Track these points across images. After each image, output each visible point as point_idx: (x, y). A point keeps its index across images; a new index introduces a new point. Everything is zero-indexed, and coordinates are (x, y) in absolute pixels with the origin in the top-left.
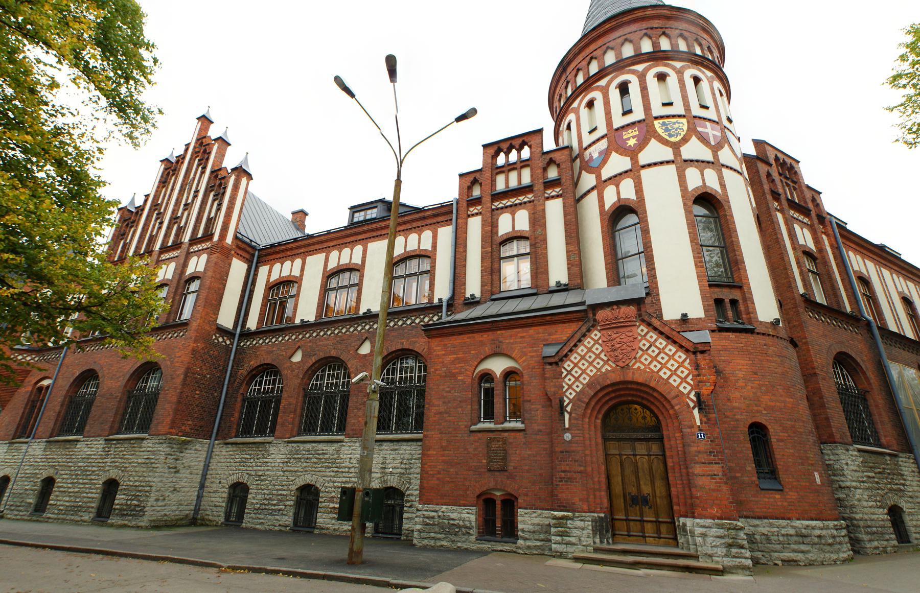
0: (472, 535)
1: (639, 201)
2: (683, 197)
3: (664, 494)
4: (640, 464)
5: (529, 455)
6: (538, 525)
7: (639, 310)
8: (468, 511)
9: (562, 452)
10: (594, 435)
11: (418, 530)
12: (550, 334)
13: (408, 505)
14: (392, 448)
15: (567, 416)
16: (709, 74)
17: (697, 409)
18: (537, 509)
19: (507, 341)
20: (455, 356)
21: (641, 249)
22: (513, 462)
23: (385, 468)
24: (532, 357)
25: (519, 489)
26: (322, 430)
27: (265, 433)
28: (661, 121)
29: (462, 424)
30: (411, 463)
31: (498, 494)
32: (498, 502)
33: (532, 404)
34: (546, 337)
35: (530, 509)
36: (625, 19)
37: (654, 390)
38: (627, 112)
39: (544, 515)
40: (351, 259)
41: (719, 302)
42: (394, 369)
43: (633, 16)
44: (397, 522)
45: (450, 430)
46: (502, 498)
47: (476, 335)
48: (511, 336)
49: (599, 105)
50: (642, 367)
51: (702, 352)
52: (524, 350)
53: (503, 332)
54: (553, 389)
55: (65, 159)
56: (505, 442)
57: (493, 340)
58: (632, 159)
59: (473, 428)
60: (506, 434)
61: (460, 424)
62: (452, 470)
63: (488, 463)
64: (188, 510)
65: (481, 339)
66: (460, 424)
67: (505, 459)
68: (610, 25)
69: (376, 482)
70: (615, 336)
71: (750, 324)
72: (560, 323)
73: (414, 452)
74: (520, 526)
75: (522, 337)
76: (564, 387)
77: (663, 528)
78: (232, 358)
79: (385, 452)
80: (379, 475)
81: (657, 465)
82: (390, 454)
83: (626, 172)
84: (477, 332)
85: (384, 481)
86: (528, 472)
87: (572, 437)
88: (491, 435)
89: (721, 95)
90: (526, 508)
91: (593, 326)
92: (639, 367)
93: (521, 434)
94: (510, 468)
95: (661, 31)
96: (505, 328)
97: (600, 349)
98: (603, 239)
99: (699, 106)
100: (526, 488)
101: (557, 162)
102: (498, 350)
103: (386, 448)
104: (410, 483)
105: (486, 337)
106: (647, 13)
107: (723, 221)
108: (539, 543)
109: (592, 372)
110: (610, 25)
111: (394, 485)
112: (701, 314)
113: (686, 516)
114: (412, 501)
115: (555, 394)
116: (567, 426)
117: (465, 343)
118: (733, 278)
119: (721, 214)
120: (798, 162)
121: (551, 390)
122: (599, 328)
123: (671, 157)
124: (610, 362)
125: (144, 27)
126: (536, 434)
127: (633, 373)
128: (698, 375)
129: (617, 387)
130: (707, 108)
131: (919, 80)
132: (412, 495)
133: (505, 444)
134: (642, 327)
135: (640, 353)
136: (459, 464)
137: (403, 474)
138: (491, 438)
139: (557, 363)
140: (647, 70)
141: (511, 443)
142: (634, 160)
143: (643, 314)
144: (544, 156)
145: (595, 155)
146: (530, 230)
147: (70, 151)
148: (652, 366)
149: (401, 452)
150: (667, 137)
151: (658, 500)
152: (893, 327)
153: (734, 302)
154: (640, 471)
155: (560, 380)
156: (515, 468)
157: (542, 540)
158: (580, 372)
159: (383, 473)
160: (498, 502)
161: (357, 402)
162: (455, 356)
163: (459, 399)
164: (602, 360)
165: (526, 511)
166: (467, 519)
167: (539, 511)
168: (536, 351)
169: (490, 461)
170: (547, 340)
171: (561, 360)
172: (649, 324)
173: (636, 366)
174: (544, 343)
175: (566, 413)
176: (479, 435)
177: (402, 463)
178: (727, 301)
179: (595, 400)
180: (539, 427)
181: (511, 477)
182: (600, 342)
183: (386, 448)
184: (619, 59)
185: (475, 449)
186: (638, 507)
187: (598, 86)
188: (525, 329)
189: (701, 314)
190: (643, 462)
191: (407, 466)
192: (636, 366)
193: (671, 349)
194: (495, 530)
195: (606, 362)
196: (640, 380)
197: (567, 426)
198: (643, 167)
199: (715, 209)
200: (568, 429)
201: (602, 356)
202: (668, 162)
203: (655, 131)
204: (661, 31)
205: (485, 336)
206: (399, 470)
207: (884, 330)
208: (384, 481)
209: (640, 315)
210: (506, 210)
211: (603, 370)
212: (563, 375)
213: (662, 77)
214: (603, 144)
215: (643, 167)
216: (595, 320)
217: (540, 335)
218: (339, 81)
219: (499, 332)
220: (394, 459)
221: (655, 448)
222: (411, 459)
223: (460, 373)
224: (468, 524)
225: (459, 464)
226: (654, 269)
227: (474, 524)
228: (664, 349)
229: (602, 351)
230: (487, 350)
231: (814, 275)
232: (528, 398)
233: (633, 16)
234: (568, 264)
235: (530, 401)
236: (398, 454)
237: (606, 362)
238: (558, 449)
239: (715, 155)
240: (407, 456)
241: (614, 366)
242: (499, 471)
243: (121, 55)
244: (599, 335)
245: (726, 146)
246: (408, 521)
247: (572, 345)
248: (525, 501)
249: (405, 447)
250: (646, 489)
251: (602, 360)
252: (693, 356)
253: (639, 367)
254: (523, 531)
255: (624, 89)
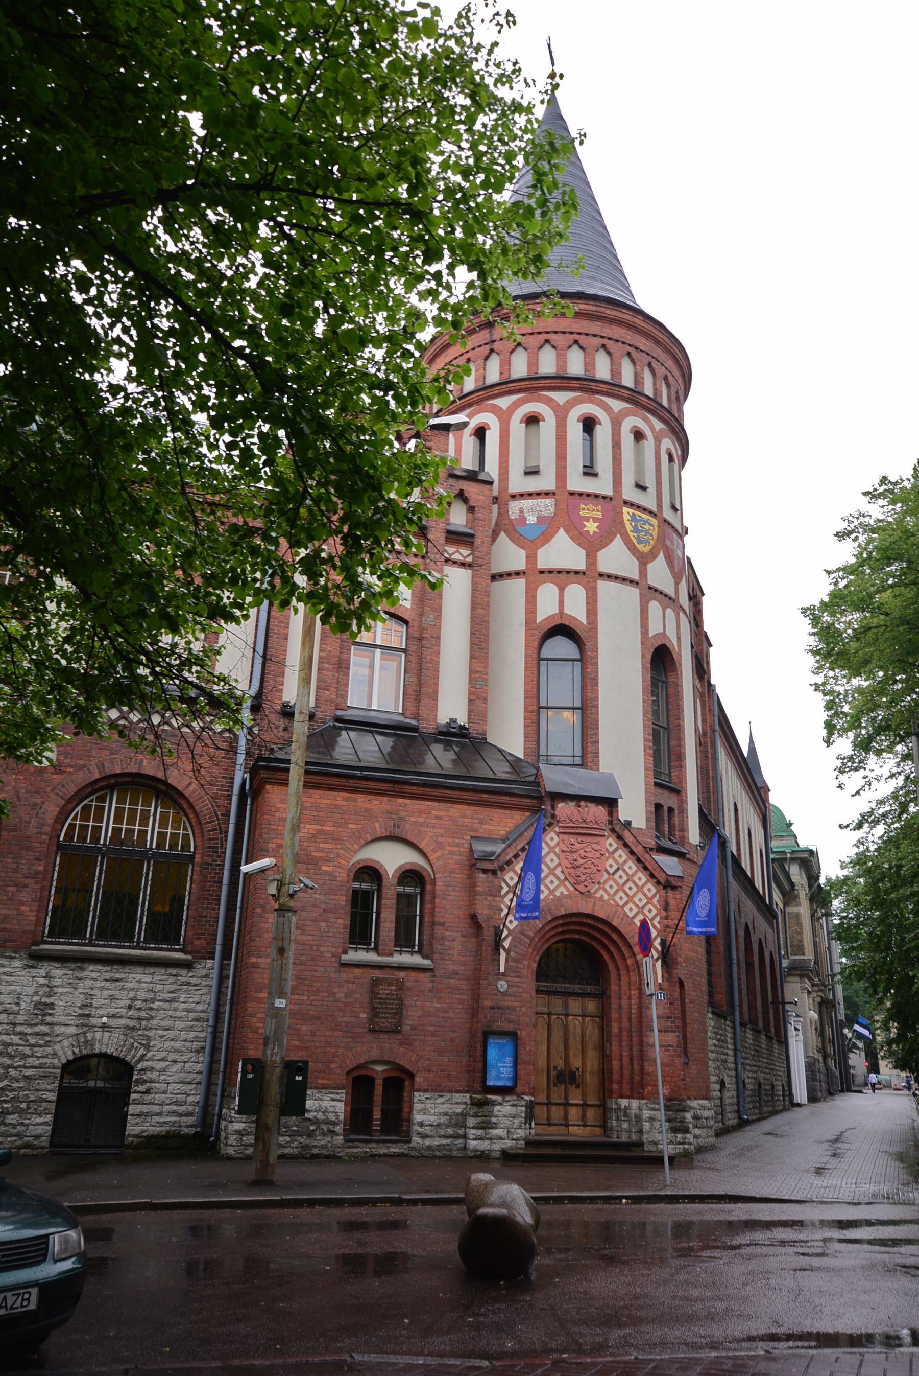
0: (338, 1135)
1: (590, 629)
2: (642, 644)
3: (596, 1068)
4: (571, 1027)
5: (437, 1009)
6: (446, 1114)
7: (610, 814)
8: (334, 1096)
9: (492, 1008)
10: (529, 983)
11: (239, 1132)
12: (481, 822)
13: (142, 1088)
14: (108, 975)
15: (503, 956)
16: (659, 425)
17: (660, 961)
18: (443, 1091)
19: (413, 819)
20: (319, 827)
21: (578, 704)
22: (412, 1016)
23: (89, 1016)
24: (452, 853)
25: (418, 1061)
26: (103, 934)
27: (79, 933)
28: (631, 511)
29: (327, 951)
30: (151, 1009)
31: (380, 1068)
32: (379, 1082)
33: (446, 930)
34: (476, 826)
35: (433, 1091)
36: (608, 312)
37: (615, 929)
38: (532, 472)
39: (454, 1100)
40: (561, 602)
41: (658, 807)
42: (100, 810)
43: (620, 315)
44: (576, 988)
45: (304, 958)
46: (386, 1075)
47: (360, 798)
48: (420, 812)
49: (548, 427)
50: (606, 897)
51: (674, 888)
52: (440, 839)
53: (408, 801)
54: (486, 912)
55: (260, 316)
56: (400, 986)
57: (388, 812)
58: (588, 555)
59: (345, 958)
60: (402, 974)
61: (322, 949)
62: (304, 1028)
63: (371, 1020)
64: (188, 1125)
65: (368, 806)
66: (322, 949)
67: (399, 1012)
68: (594, 308)
69: (66, 1043)
70: (578, 846)
71: (683, 845)
72: (498, 807)
73: (159, 987)
74: (418, 1118)
75: (439, 818)
76: (502, 910)
77: (591, 1114)
78: (239, 905)
79: (89, 983)
80: (72, 1030)
81: (592, 1031)
82: (102, 988)
83: (577, 573)
84: (362, 793)
85: (86, 1042)
86: (433, 1034)
87: (509, 986)
88: (378, 974)
89: (671, 459)
90: (426, 1091)
91: (550, 825)
92: (602, 897)
93: (427, 975)
94: (406, 1028)
95: (544, 337)
96: (412, 797)
97: (556, 861)
98: (526, 668)
99: (633, 483)
100: (429, 1059)
101: (472, 503)
102: (397, 832)
103: (94, 975)
104: (147, 1047)
105: (377, 804)
106: (637, 321)
107: (671, 691)
108: (445, 1141)
109: (621, 899)
110: (594, 308)
111: (111, 1050)
112: (643, 826)
113: (631, 1097)
114: (151, 1081)
115: (489, 918)
116: (502, 970)
117: (337, 807)
118: (670, 775)
119: (671, 679)
120: (710, 645)
121: (483, 912)
122: (557, 829)
123: (635, 576)
124: (567, 883)
125: (812, 641)
126: (449, 978)
127: (595, 904)
128: (666, 918)
129: (569, 920)
130: (644, 489)
131: (194, 9)
132: (152, 1069)
133: (401, 989)
134: (610, 840)
135: (606, 876)
136: (318, 1018)
137: (133, 1029)
138: (378, 979)
139: (494, 872)
140: (571, 404)
141: (409, 989)
142: (591, 558)
143: (615, 822)
144: (452, 481)
145: (531, 519)
146: (412, 608)
147: (151, 410)
148: (617, 898)
149: (128, 985)
150: (635, 541)
151: (588, 1075)
152: (745, 864)
153: (671, 810)
154: (571, 1036)
155: (497, 899)
156: (414, 1028)
157: (450, 1137)
158: (621, 894)
159: (83, 1025)
160: (379, 1082)
161: (15, 871)
162: (319, 827)
163: (323, 906)
164: (558, 878)
165: (428, 1095)
166: (331, 1109)
167: (448, 1096)
168: (458, 845)
169: (374, 1013)
170: (476, 830)
171: (502, 869)
172: (619, 837)
173: (598, 895)
174: (472, 834)
175: (502, 951)
176: (357, 971)
177: (130, 1007)
178: (666, 808)
179: (551, 926)
180: (455, 967)
181: (407, 1042)
182: (557, 850)
183: (94, 975)
184: (505, 376)
185: (348, 995)
186: (563, 1087)
187: (551, 400)
188: (444, 805)
189: (643, 826)
190: (575, 1023)
191: (143, 1014)
192: (598, 895)
193: (641, 877)
194: (371, 1125)
195: (562, 883)
196: (602, 915)
197: (502, 970)
198: (513, 497)
199: (665, 669)
200: (503, 974)
201: (558, 872)
202: (547, 494)
203: (622, 522)
204: (488, 347)
205: (375, 802)
206: (122, 1022)
207: (736, 861)
208: (86, 1042)
209: (610, 822)
210: (596, 501)
211: (558, 894)
212: (503, 892)
213: (532, 420)
214: (547, 506)
215: (513, 497)
216: (553, 816)
217: (467, 820)
218: (841, 827)
219: (400, 801)
220: (112, 998)
221: (591, 1006)
222: (153, 1001)
223: (327, 860)
224: (332, 1117)
225: (318, 1018)
226: (597, 742)
227: (342, 1117)
228: (633, 875)
229: (559, 864)
230: (379, 828)
231: (658, 399)
232: (441, 920)
233: (620, 315)
234: (470, 693)
235: (443, 924)
236: (123, 989)
237: (562, 883)
238: (487, 1003)
239: (643, 572)
240: (142, 995)
241: (572, 889)
242: (388, 1032)
243: (288, 34)
244: (556, 839)
245: (618, 539)
246: (138, 1120)
247: (519, 847)
248: (425, 1079)
249: (138, 977)
250: (576, 1063)
251: (558, 878)
252: (663, 892)
253: (602, 897)
254: (421, 1124)
255: (589, 424)
